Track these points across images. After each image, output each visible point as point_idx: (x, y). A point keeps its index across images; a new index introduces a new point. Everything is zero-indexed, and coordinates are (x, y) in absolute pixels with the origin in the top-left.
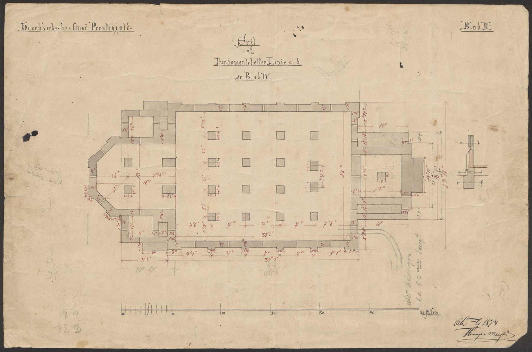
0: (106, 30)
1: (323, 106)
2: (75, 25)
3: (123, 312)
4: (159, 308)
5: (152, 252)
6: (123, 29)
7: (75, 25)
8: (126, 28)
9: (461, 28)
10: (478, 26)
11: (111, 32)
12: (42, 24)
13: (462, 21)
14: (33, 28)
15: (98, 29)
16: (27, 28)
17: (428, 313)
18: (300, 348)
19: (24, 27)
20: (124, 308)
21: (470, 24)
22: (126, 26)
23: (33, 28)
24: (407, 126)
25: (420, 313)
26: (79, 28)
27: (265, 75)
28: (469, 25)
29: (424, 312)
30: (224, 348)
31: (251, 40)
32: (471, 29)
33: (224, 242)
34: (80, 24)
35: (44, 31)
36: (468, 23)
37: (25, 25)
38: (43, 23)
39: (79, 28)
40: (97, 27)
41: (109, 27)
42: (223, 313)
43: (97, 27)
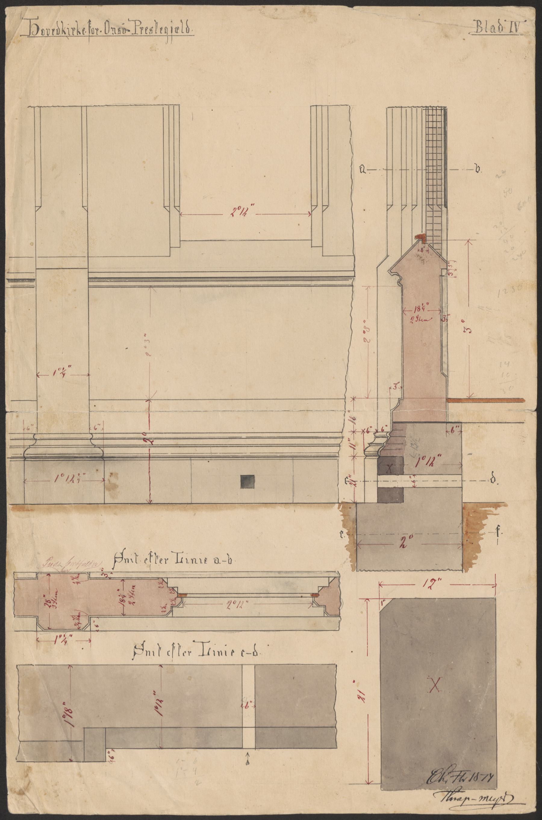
0: (156, 33)
1: (97, 425)
6: (179, 31)
8: (184, 30)
9: (525, 23)
10: (186, 27)
11: (163, 36)
12: (487, 31)
14: (48, 30)
15: (144, 31)
16: (40, 32)
18: (535, 414)
19: (34, 29)
23: (48, 30)
24: (122, 581)
27: (513, 23)
30: (355, 7)
32: (183, 33)
33: (500, 504)
35: (183, 34)
37: (36, 25)
38: (209, 641)
41: (161, 29)
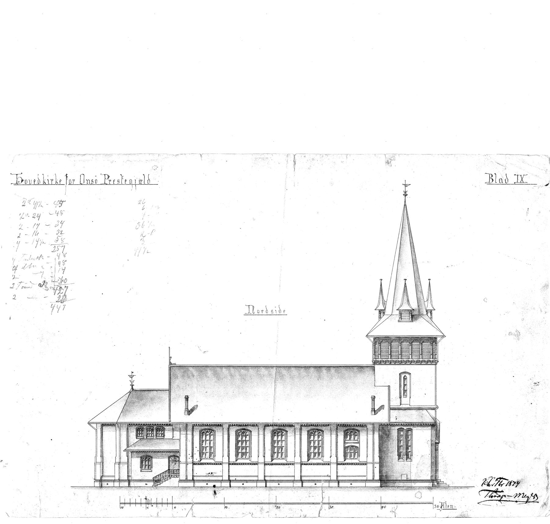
2: (82, 176)
3: (122, 505)
4: (160, 501)
5: (165, 437)
7: (82, 176)
13: (11, 174)
17: (443, 507)
20: (123, 501)
21: (494, 175)
22: (146, 179)
25: (435, 507)
26: (88, 181)
28: (494, 178)
29: (438, 506)
31: (276, 309)
34: (89, 176)
36: (492, 176)
37: (108, 175)
39: (88, 181)
40: (110, 181)
42: (226, 507)
43: (110, 181)
